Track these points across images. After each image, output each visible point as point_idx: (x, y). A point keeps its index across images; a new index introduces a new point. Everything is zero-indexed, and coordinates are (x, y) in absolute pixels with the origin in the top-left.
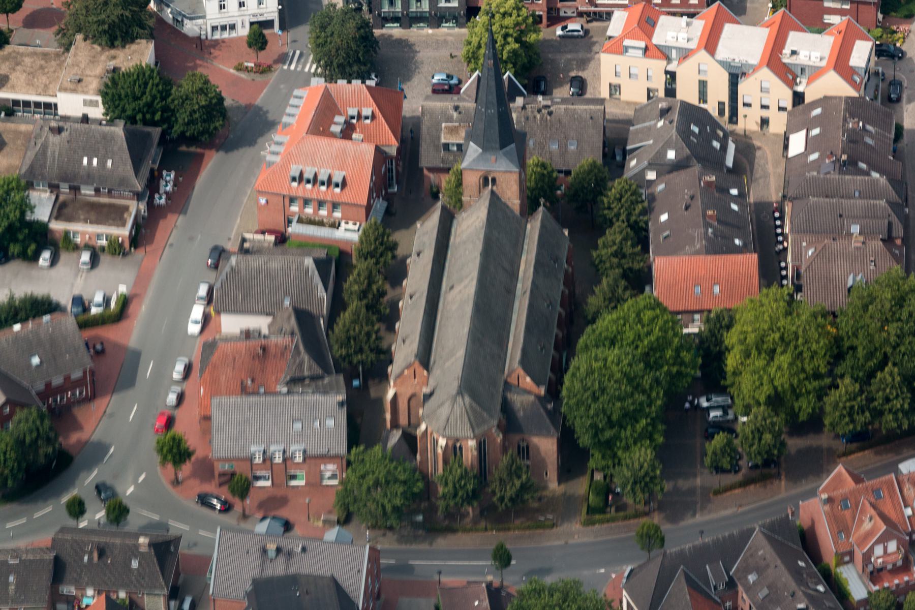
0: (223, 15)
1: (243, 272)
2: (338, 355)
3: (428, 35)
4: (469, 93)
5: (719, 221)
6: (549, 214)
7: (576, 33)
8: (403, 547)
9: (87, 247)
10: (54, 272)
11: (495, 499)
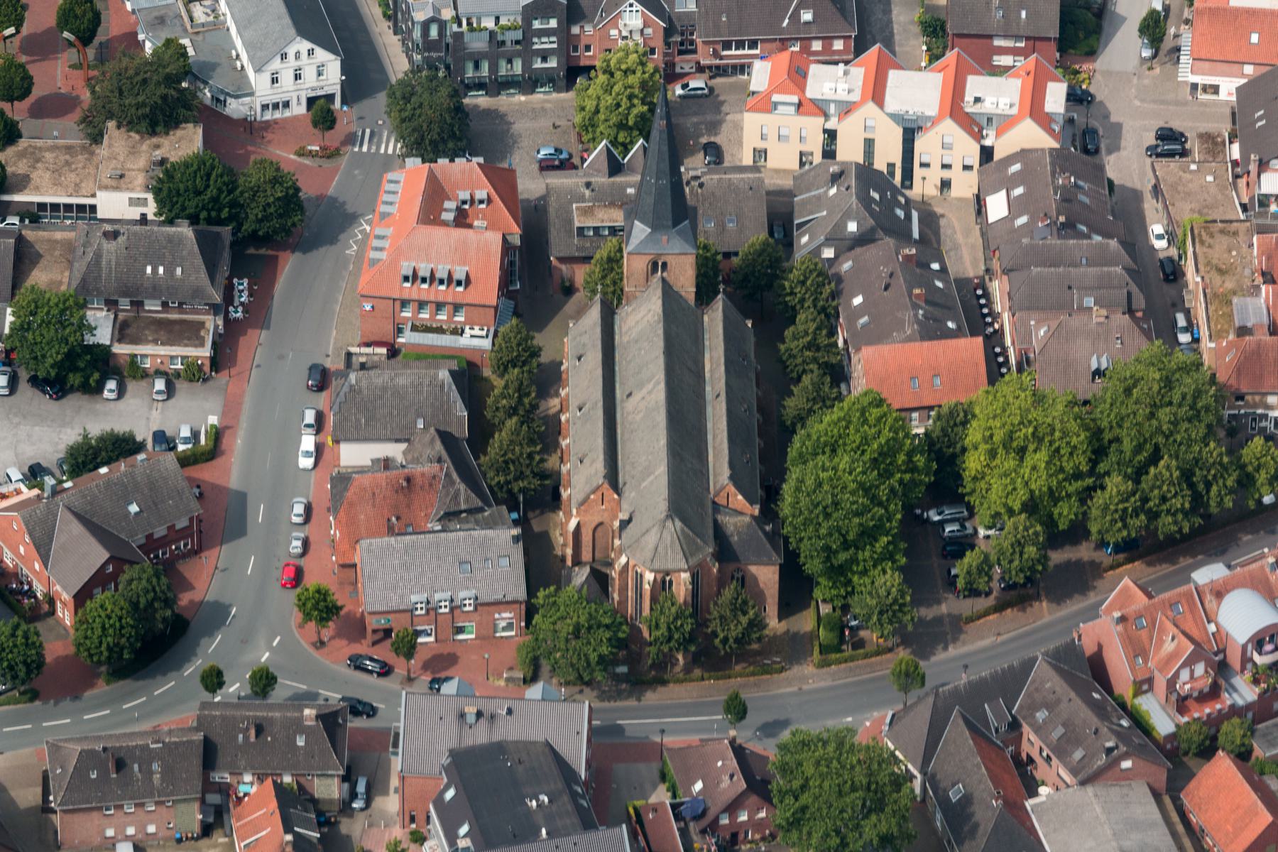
0: (275, 91)
1: (365, 392)
2: (493, 483)
3: (521, 103)
4: (596, 167)
5: (927, 302)
6: (729, 303)
7: (699, 92)
8: (606, 704)
9: (159, 373)
10: (121, 404)
11: (717, 641)
